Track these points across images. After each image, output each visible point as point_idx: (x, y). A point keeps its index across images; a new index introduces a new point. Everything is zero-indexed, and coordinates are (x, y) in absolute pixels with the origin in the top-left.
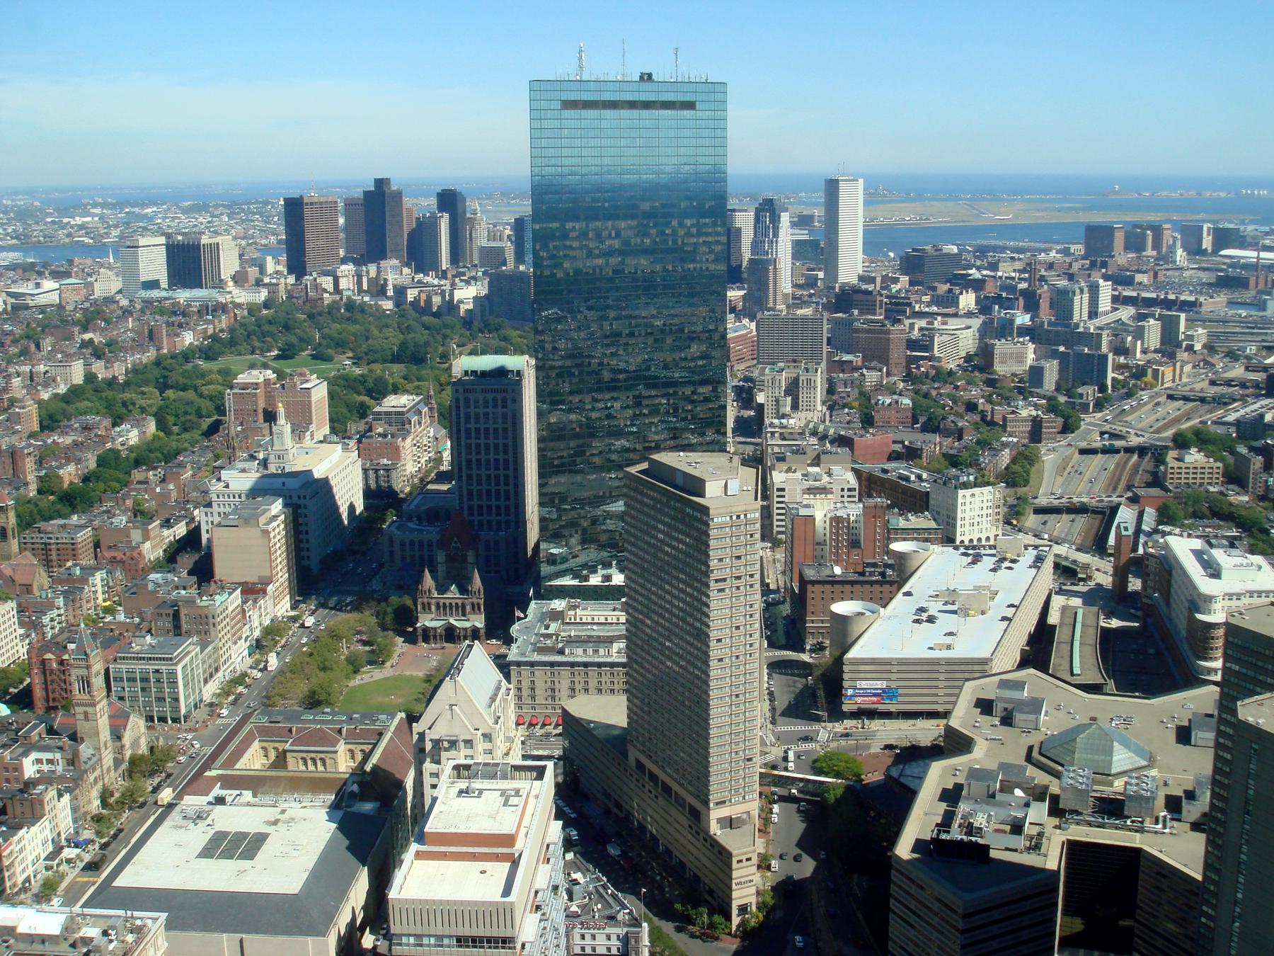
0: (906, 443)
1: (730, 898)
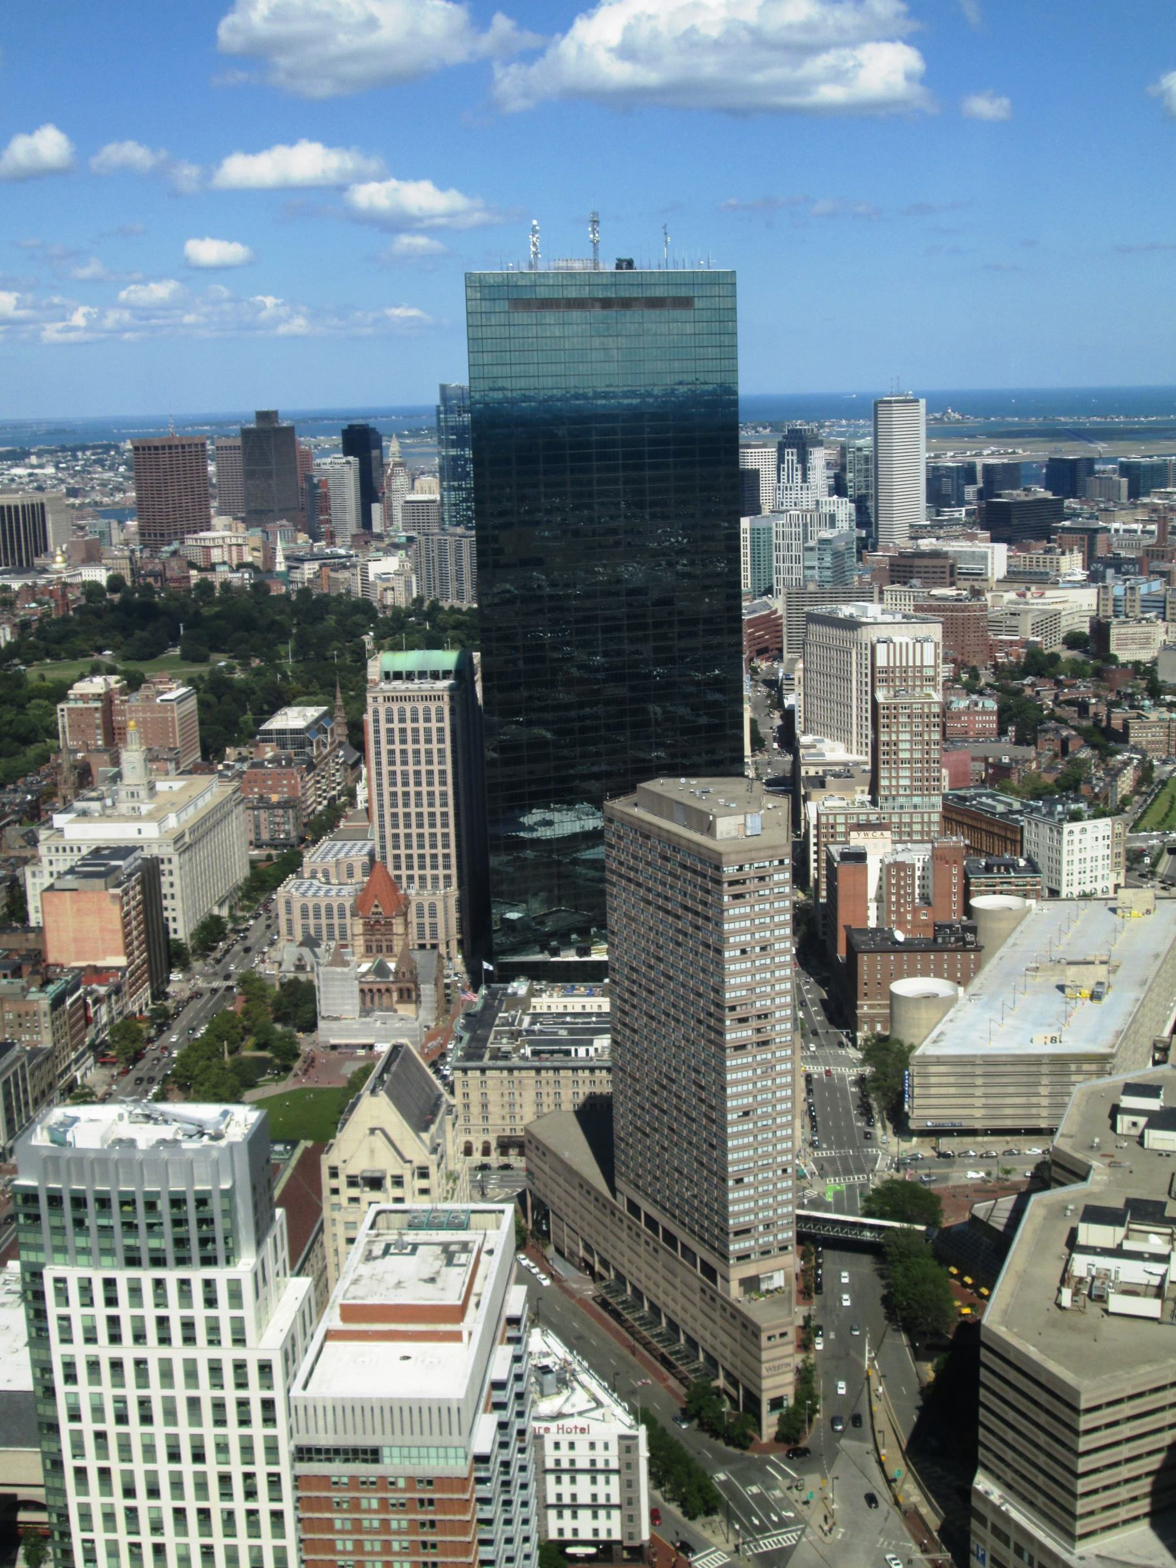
1: (760, 1390)
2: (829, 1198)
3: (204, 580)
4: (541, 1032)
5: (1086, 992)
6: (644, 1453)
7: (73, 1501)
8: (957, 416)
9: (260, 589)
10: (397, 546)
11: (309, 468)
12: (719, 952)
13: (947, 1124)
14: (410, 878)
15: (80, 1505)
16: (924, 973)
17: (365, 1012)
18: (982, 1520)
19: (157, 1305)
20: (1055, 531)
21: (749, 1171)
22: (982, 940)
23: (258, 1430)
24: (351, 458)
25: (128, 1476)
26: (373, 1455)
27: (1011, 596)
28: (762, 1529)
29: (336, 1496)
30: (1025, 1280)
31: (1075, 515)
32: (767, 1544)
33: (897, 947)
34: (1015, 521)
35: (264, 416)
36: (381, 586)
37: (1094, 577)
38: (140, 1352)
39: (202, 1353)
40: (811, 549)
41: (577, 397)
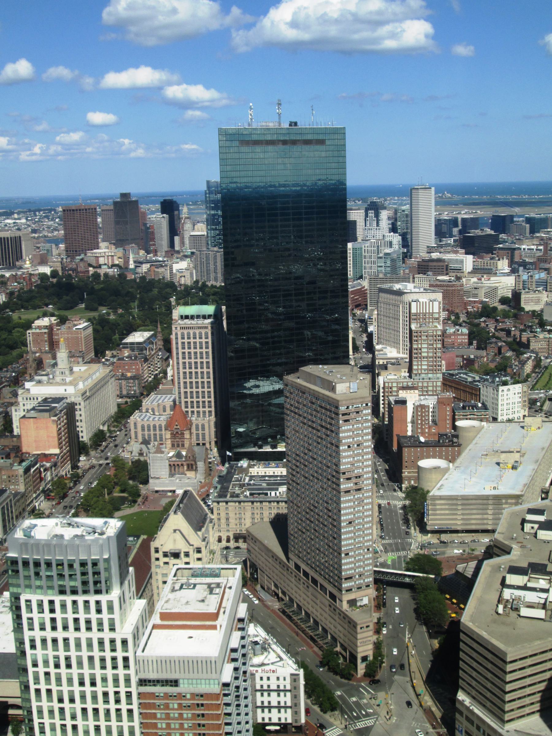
1: (357, 652)
2: (389, 562)
3: (96, 272)
4: (254, 485)
5: (510, 466)
6: (302, 682)
7: (34, 704)
8: (449, 195)
9: (122, 276)
10: (186, 256)
11: (145, 220)
12: (337, 447)
13: (445, 528)
14: (193, 412)
15: (37, 706)
16: (434, 457)
17: (172, 475)
18: (461, 713)
19: (74, 613)
20: (495, 249)
21: (351, 550)
22: (461, 441)
23: (121, 671)
24: (165, 215)
25: (60, 693)
26: (175, 683)
27: (475, 280)
28: (358, 718)
29: (158, 702)
30: (481, 601)
31: (504, 242)
32: (360, 725)
33: (421, 445)
34: (476, 245)
35: (124, 195)
36: (179, 275)
37: (514, 271)
38: (66, 635)
39: (95, 635)
40: (381, 258)
41: (271, 186)
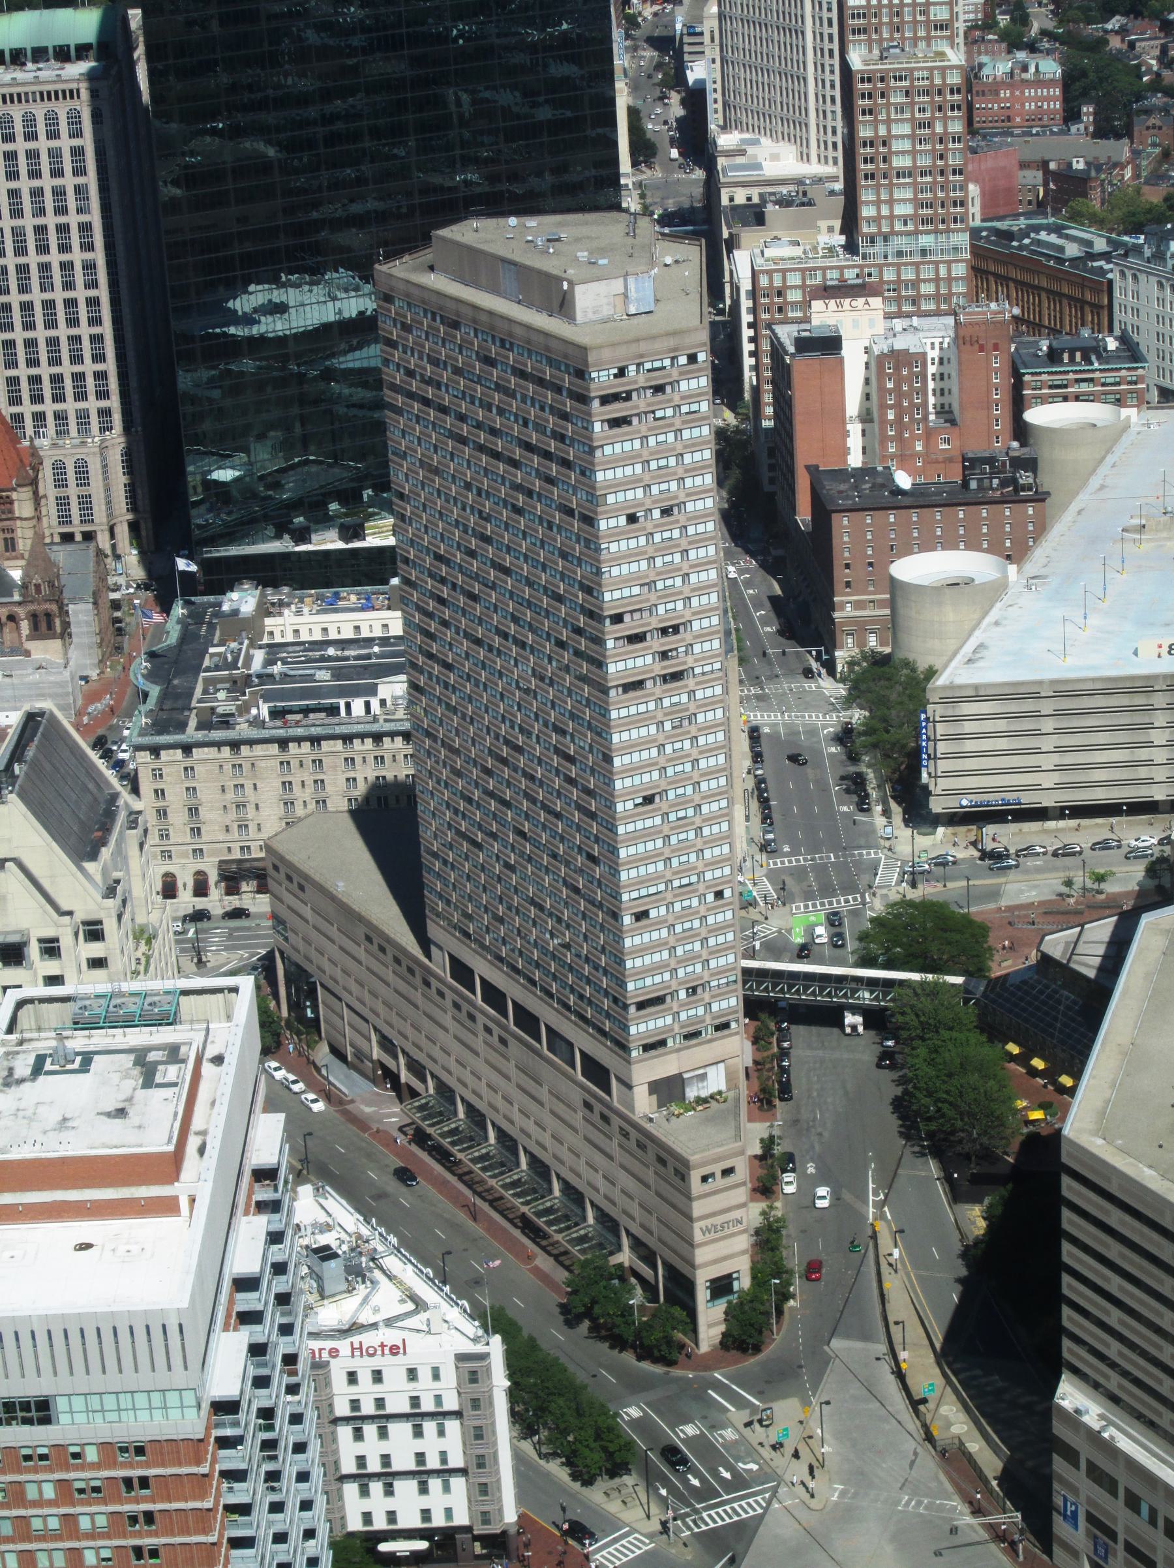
0: (1053, 166)
4: (285, 677)
6: (500, 1381)
12: (589, 521)
18: (1072, 1456)
22: (1046, 481)
28: (706, 1493)
32: (715, 1518)
33: (898, 500)
